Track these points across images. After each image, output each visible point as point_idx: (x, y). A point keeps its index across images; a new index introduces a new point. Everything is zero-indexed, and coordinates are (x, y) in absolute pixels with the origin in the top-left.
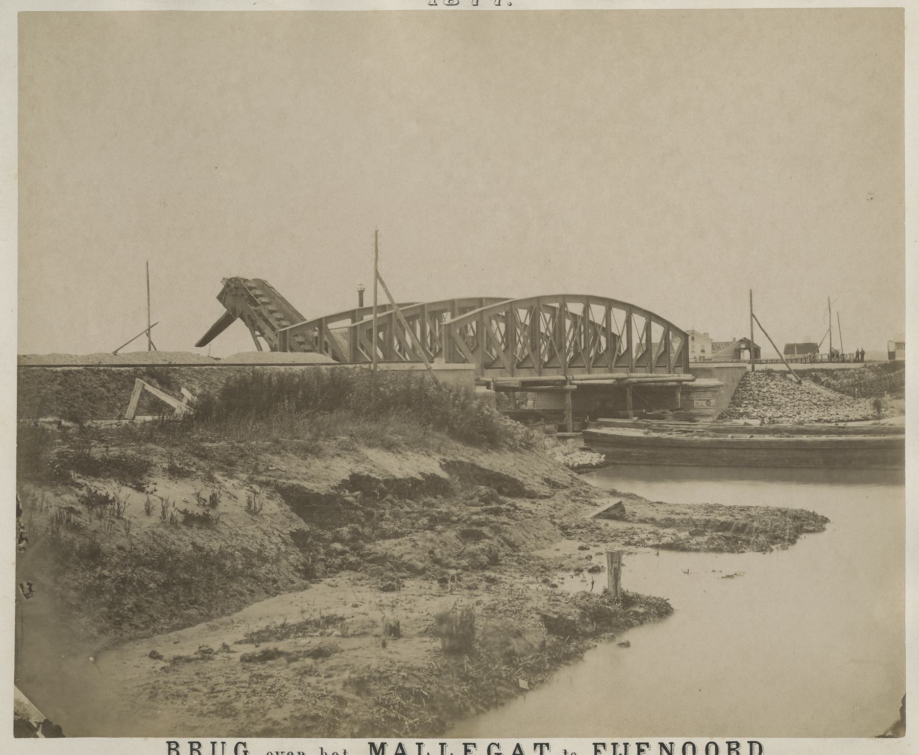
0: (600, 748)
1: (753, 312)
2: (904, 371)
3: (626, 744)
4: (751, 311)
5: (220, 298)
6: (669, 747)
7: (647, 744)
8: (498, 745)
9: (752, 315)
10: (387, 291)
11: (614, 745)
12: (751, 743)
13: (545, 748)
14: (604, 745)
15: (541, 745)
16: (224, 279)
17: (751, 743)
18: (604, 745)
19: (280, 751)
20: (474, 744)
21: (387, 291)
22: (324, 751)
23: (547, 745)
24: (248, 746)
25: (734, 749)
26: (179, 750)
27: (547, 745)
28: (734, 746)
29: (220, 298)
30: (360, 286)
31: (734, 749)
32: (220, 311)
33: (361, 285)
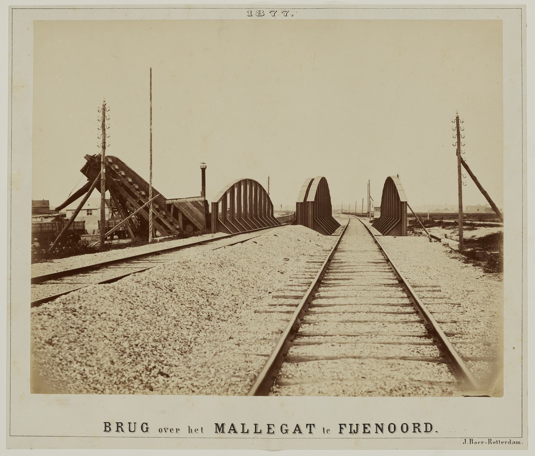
0: (343, 426)
1: (463, 156)
2: (501, 253)
3: (357, 425)
4: (458, 153)
5: (83, 171)
6: (381, 426)
7: (369, 425)
8: (286, 425)
9: (461, 161)
10: (411, 209)
11: (351, 425)
12: (426, 424)
13: (312, 426)
14: (345, 425)
15: (310, 425)
16: (87, 155)
17: (426, 424)
18: (345, 425)
19: (166, 428)
20: (274, 425)
21: (411, 209)
22: (190, 428)
23: (314, 425)
24: (148, 424)
25: (417, 427)
26: (111, 427)
27: (314, 425)
28: (417, 425)
29: (83, 171)
30: (202, 165)
31: (417, 427)
32: (84, 181)
33: (203, 163)
